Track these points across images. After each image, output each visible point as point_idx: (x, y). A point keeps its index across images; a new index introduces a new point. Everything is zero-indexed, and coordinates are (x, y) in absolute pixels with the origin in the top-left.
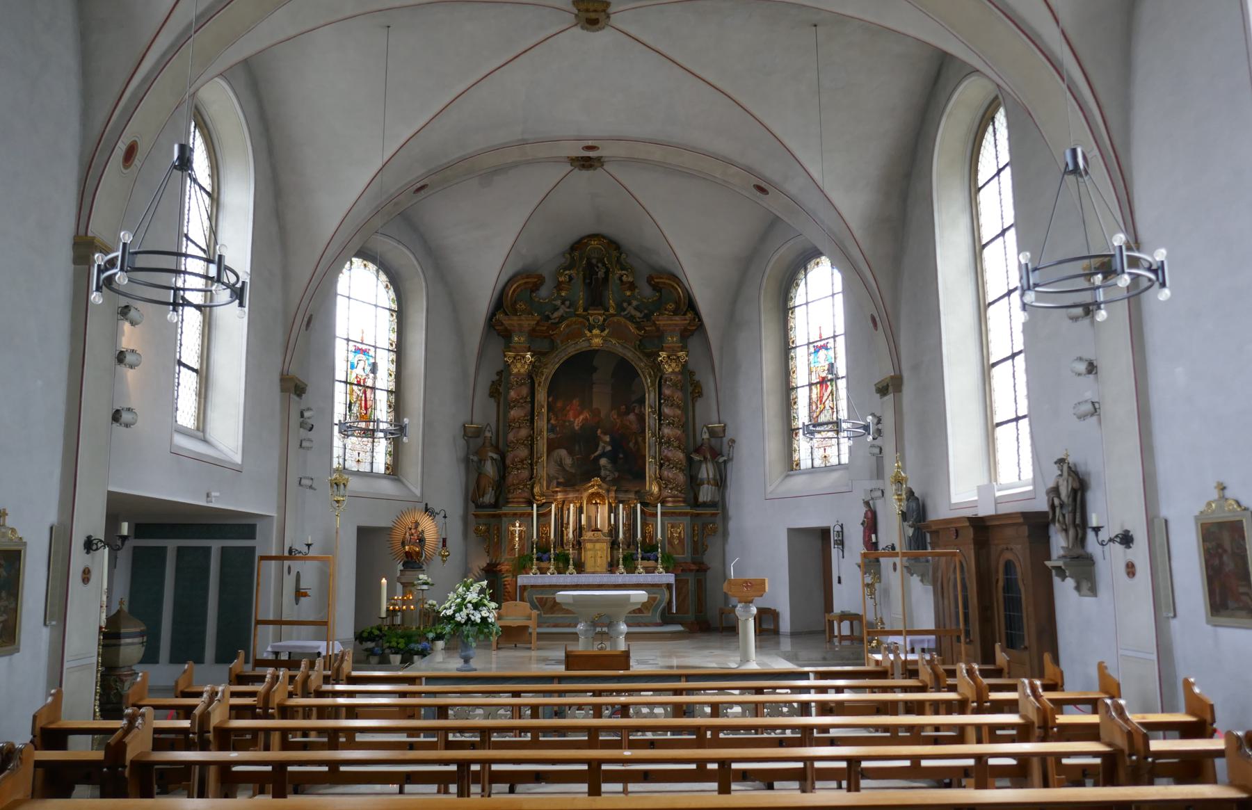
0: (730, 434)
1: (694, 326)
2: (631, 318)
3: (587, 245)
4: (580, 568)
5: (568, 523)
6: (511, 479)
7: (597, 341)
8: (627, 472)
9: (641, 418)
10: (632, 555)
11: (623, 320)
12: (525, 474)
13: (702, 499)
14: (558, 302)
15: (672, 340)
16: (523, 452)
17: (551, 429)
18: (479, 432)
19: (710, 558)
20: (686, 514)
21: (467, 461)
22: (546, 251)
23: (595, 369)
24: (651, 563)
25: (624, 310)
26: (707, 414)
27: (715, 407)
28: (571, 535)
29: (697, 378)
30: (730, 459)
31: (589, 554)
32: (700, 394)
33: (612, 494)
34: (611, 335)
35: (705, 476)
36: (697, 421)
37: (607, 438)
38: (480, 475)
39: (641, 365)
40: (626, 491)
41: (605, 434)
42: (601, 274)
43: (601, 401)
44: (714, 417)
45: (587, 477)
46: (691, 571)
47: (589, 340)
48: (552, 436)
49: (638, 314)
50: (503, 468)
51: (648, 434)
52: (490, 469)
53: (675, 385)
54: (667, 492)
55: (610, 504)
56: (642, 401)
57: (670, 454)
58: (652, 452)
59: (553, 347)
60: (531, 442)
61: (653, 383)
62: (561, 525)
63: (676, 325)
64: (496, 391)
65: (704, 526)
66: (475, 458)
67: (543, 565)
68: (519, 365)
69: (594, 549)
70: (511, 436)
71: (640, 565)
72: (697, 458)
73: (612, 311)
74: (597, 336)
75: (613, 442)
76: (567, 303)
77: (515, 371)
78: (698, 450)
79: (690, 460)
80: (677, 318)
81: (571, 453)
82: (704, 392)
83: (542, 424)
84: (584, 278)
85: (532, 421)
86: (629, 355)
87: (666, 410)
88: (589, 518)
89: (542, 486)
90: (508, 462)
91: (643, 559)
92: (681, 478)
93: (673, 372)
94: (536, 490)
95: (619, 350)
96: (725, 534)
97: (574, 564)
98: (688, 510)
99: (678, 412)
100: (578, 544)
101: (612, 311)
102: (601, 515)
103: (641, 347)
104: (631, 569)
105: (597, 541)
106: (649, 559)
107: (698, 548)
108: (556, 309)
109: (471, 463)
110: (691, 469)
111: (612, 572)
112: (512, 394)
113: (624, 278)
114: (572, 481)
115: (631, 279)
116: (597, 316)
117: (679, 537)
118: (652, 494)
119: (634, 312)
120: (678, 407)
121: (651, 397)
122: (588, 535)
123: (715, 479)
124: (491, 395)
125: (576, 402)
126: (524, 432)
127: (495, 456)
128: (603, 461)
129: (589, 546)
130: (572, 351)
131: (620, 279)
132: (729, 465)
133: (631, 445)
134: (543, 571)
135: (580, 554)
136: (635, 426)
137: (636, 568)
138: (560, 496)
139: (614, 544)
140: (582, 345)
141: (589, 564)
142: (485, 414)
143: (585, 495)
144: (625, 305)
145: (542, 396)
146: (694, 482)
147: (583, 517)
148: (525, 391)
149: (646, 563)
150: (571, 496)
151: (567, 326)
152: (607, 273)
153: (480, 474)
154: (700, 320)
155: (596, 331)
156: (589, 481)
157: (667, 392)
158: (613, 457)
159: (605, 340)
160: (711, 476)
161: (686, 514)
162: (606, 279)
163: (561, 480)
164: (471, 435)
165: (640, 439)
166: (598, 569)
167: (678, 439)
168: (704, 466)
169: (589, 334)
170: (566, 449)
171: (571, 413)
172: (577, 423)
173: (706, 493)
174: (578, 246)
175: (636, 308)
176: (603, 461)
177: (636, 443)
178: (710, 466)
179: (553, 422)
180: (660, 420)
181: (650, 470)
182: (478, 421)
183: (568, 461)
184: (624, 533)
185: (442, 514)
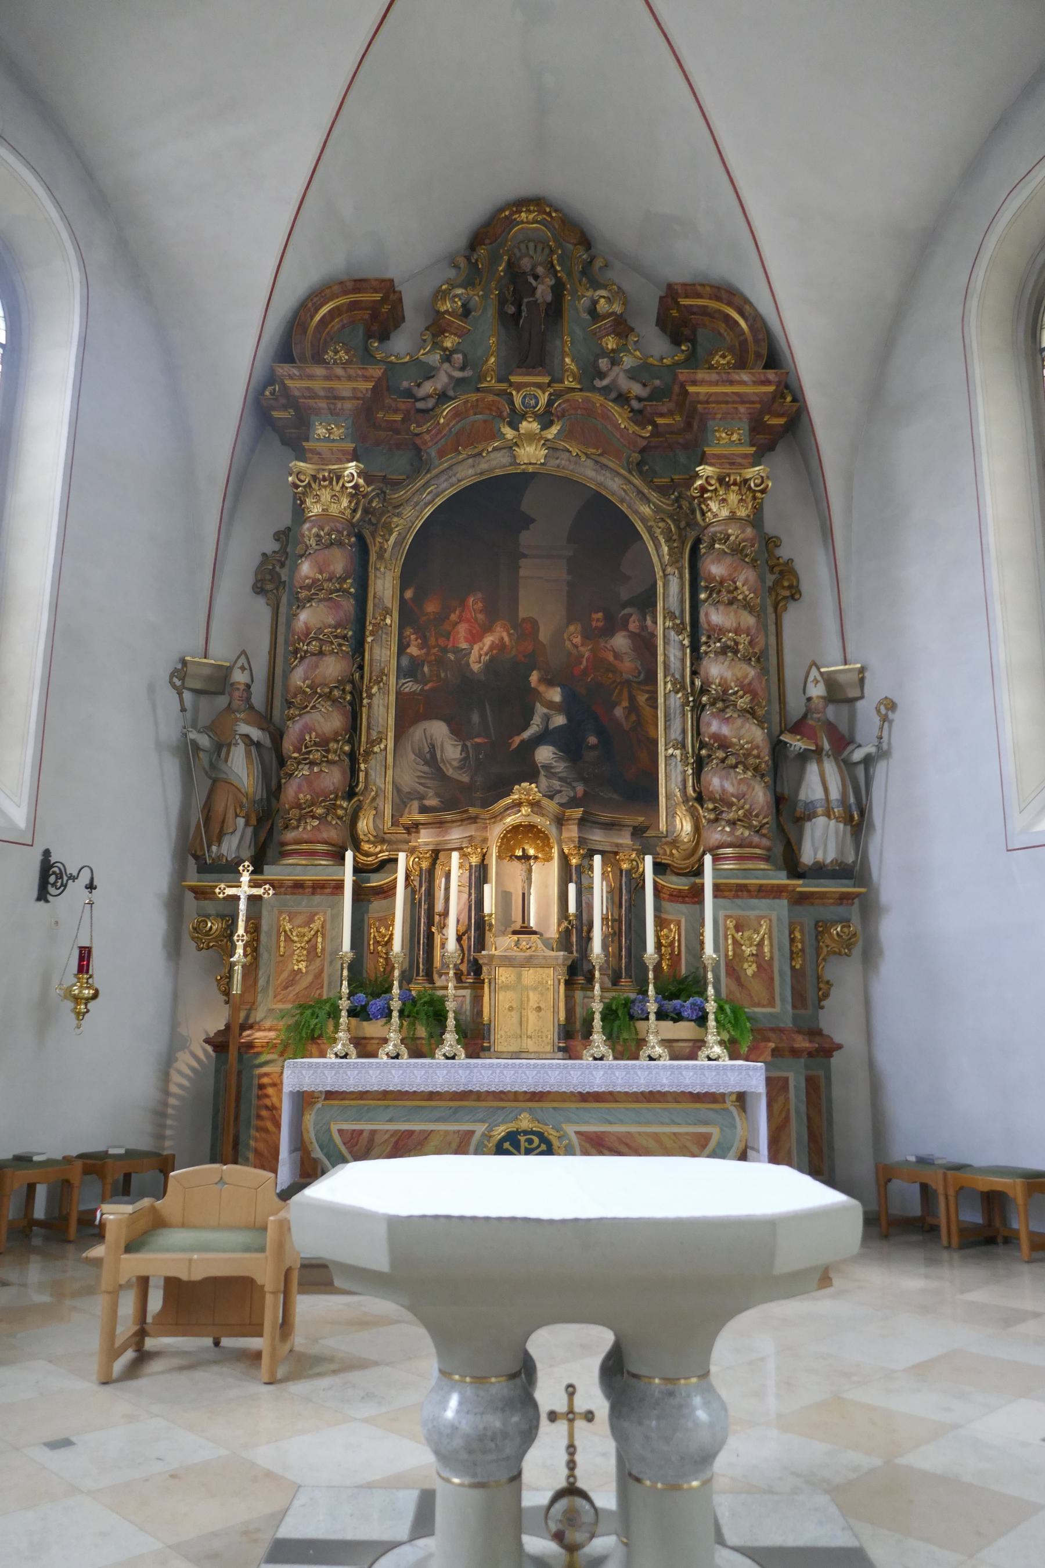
0: (875, 690)
1: (781, 424)
2: (622, 399)
3: (511, 223)
4: (476, 1039)
5: (445, 914)
6: (293, 791)
7: (531, 454)
8: (611, 777)
9: (645, 645)
10: (628, 1004)
11: (598, 399)
12: (333, 778)
13: (808, 855)
14: (435, 358)
15: (728, 439)
16: (328, 720)
17: (410, 671)
18: (218, 682)
19: (840, 1022)
20: (775, 892)
21: (187, 753)
22: (411, 240)
23: (527, 521)
24: (684, 1030)
25: (602, 375)
26: (815, 646)
27: (831, 625)
28: (452, 945)
29: (784, 553)
30: (882, 753)
31: (505, 998)
32: (795, 594)
33: (572, 831)
34: (567, 434)
35: (818, 794)
36: (788, 658)
37: (555, 695)
38: (216, 781)
39: (643, 511)
40: (610, 826)
41: (550, 683)
42: (543, 291)
43: (541, 600)
44: (836, 653)
45: (500, 787)
46: (795, 1053)
47: (510, 447)
48: (410, 687)
49: (636, 389)
50: (274, 762)
51: (663, 686)
52: (241, 769)
53: (737, 551)
54: (716, 835)
55: (564, 858)
56: (647, 602)
57: (725, 730)
58: (675, 734)
59: (419, 464)
60: (352, 699)
61: (675, 560)
62: (425, 918)
63: (742, 399)
64: (271, 580)
65: (821, 928)
66: (204, 741)
67: (372, 1029)
68: (326, 495)
69: (517, 985)
70: (298, 677)
71: (656, 1032)
72: (797, 743)
73: (569, 383)
74: (531, 438)
75: (571, 705)
76: (458, 357)
77: (316, 510)
78: (798, 727)
79: (778, 748)
80: (745, 376)
81: (458, 731)
82: (805, 587)
83: (383, 653)
84: (502, 301)
85: (359, 647)
86: (614, 484)
87: (715, 616)
88: (504, 898)
89: (379, 815)
90: (288, 745)
91: (661, 1015)
92: (760, 796)
93: (732, 518)
94: (365, 825)
95: (589, 474)
96: (871, 957)
97: (459, 1029)
98: (781, 879)
99: (748, 620)
100: (474, 972)
101: (569, 383)
102: (540, 891)
103: (643, 464)
104: (627, 1046)
105: (528, 962)
106: (677, 1018)
107: (810, 991)
108: (429, 373)
109: (199, 761)
110: (780, 767)
111: (569, 1052)
112: (306, 568)
113: (603, 306)
114: (466, 797)
115: (617, 308)
116: (531, 390)
117: (758, 956)
118: (675, 843)
119: (625, 384)
120: (747, 606)
121: (671, 591)
122: (500, 945)
123: (844, 801)
124: (259, 589)
125: (474, 602)
126: (332, 668)
127: (256, 734)
128: (545, 754)
129: (504, 975)
130: (467, 474)
131: (593, 312)
132: (880, 770)
133: (619, 712)
134: (365, 1048)
135: (477, 1000)
136: (628, 665)
137: (642, 1042)
138: (425, 838)
139: (577, 974)
140: (494, 462)
141: (503, 1036)
142: (237, 633)
143: (496, 831)
144: (603, 363)
145: (385, 585)
146: (788, 815)
147: (488, 890)
148: (339, 562)
149: (670, 1029)
150: (456, 835)
151: (457, 414)
152: (558, 289)
153: (215, 781)
154: (798, 398)
155: (529, 426)
156: (509, 793)
157: (716, 569)
158: (569, 744)
159: (552, 448)
160: (835, 794)
161: (775, 892)
162: (555, 310)
163: (432, 802)
164: (203, 687)
165: (642, 698)
166: (530, 1045)
167: (747, 689)
168: (812, 770)
169: (509, 433)
170: (448, 721)
171: (462, 629)
172: (478, 655)
173: (821, 841)
174: (488, 235)
175: (633, 374)
176: (545, 754)
177: (633, 707)
178: (830, 767)
179: (413, 650)
180: (695, 647)
181: (671, 776)
182: (221, 652)
183: (451, 752)
184: (605, 946)
185: (84, 878)
